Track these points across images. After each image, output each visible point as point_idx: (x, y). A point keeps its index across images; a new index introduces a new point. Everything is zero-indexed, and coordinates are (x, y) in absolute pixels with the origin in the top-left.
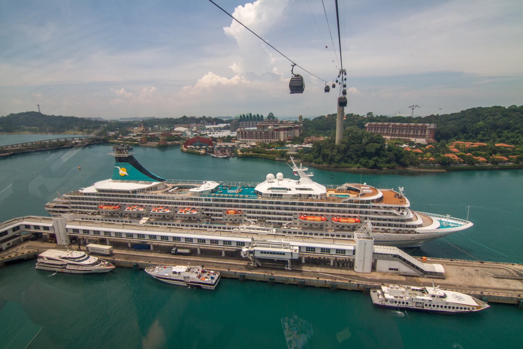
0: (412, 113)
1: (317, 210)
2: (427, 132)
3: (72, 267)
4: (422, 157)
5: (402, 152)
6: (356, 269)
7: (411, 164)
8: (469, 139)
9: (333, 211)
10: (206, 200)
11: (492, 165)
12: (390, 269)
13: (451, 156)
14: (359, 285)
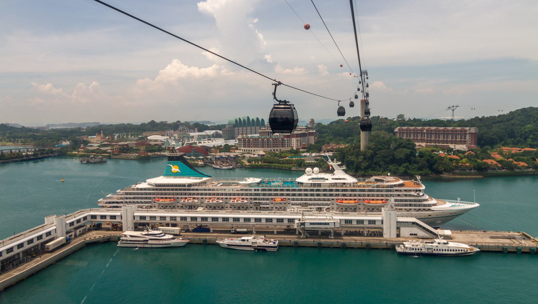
0: (453, 115)
1: (350, 195)
2: (468, 137)
3: (154, 242)
4: (457, 163)
5: (435, 158)
6: (384, 236)
7: (445, 170)
8: (517, 144)
9: (364, 195)
10: (255, 190)
11: (534, 170)
12: (411, 235)
13: (489, 161)
14: (387, 243)
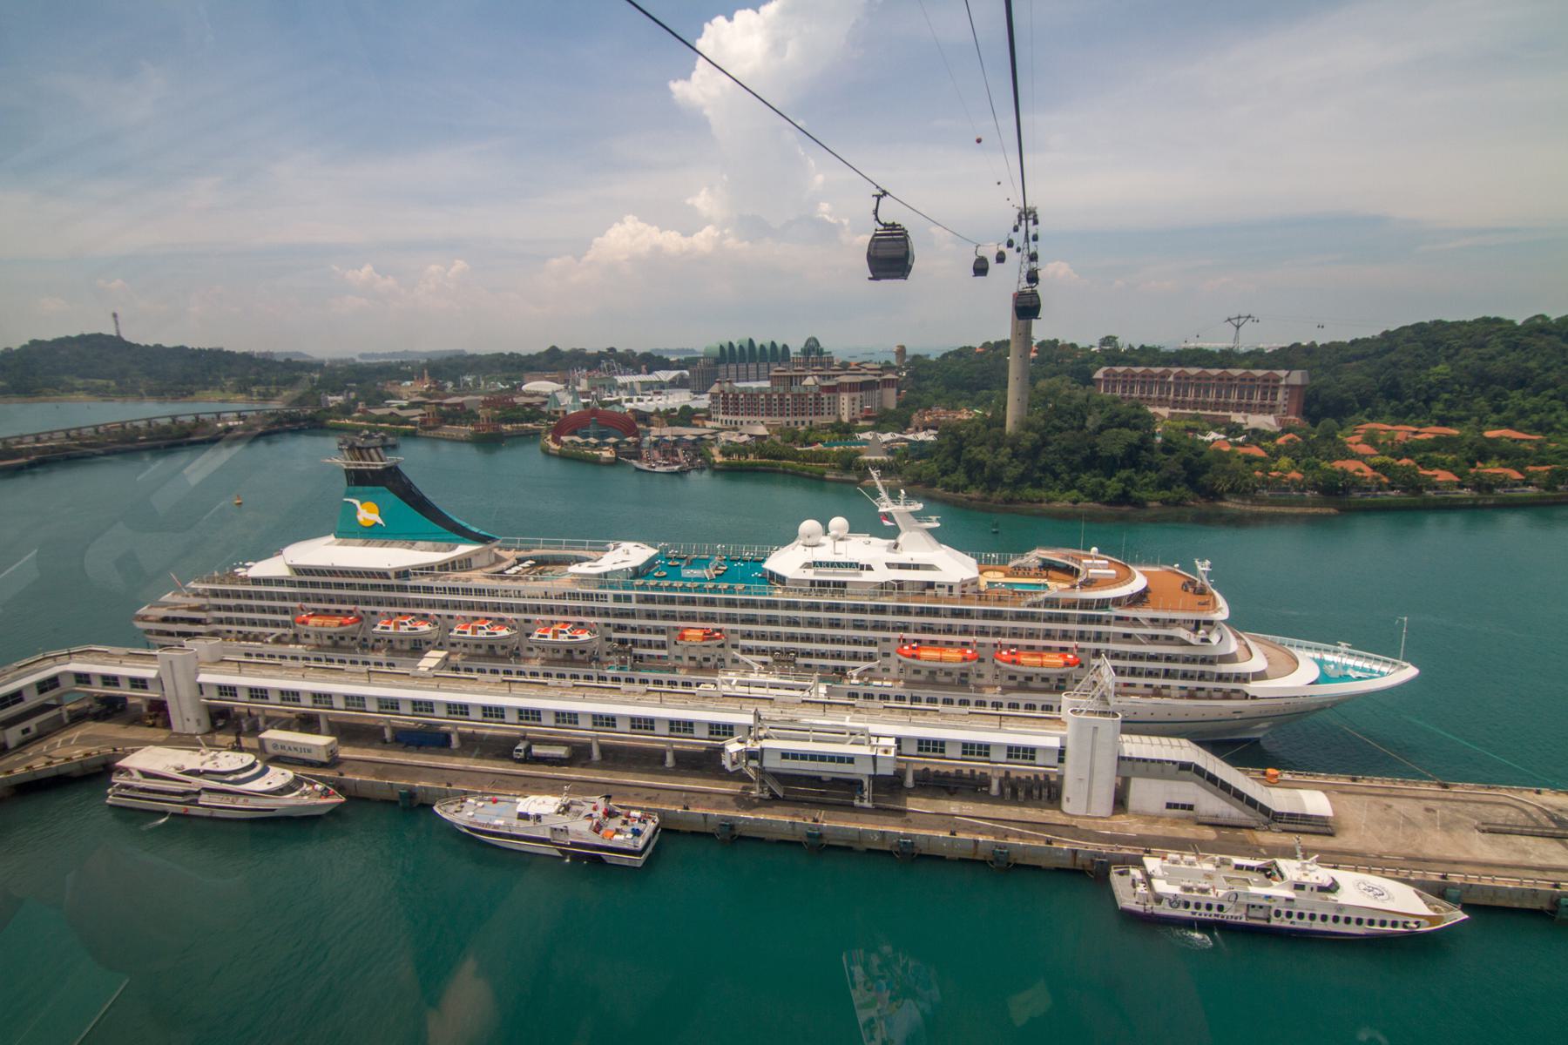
0: (1236, 339)
1: (949, 630)
2: (1280, 396)
3: (216, 801)
4: (1266, 470)
5: (1206, 456)
6: (1066, 807)
7: (1231, 490)
8: (1405, 415)
9: (998, 632)
10: (617, 598)
11: (1475, 494)
12: (1169, 806)
13: (1351, 466)
14: (1075, 852)
